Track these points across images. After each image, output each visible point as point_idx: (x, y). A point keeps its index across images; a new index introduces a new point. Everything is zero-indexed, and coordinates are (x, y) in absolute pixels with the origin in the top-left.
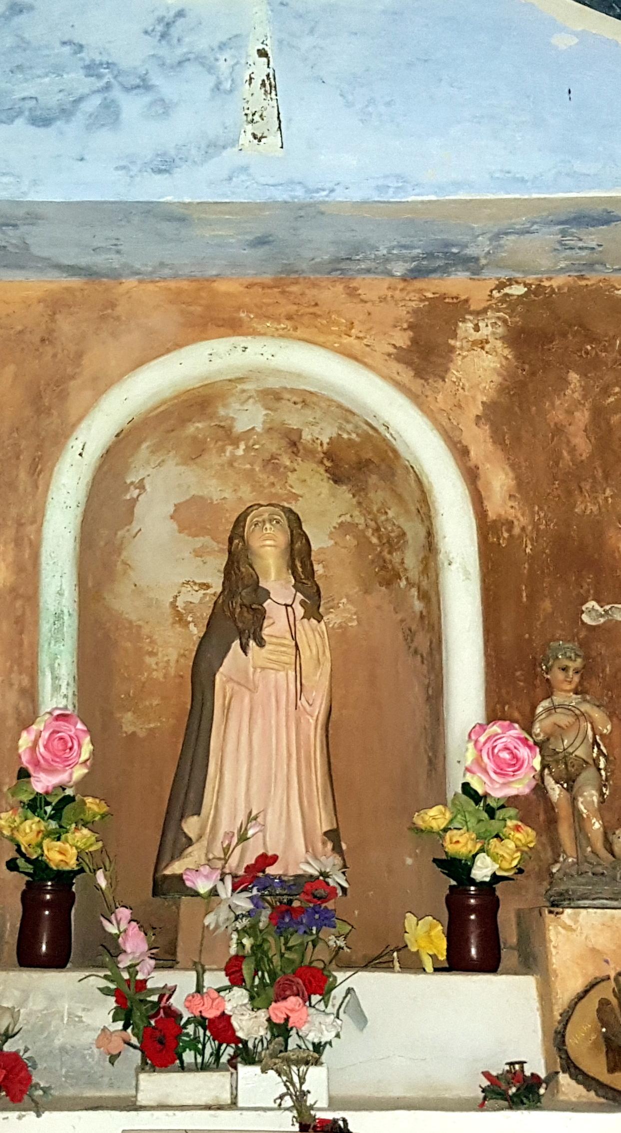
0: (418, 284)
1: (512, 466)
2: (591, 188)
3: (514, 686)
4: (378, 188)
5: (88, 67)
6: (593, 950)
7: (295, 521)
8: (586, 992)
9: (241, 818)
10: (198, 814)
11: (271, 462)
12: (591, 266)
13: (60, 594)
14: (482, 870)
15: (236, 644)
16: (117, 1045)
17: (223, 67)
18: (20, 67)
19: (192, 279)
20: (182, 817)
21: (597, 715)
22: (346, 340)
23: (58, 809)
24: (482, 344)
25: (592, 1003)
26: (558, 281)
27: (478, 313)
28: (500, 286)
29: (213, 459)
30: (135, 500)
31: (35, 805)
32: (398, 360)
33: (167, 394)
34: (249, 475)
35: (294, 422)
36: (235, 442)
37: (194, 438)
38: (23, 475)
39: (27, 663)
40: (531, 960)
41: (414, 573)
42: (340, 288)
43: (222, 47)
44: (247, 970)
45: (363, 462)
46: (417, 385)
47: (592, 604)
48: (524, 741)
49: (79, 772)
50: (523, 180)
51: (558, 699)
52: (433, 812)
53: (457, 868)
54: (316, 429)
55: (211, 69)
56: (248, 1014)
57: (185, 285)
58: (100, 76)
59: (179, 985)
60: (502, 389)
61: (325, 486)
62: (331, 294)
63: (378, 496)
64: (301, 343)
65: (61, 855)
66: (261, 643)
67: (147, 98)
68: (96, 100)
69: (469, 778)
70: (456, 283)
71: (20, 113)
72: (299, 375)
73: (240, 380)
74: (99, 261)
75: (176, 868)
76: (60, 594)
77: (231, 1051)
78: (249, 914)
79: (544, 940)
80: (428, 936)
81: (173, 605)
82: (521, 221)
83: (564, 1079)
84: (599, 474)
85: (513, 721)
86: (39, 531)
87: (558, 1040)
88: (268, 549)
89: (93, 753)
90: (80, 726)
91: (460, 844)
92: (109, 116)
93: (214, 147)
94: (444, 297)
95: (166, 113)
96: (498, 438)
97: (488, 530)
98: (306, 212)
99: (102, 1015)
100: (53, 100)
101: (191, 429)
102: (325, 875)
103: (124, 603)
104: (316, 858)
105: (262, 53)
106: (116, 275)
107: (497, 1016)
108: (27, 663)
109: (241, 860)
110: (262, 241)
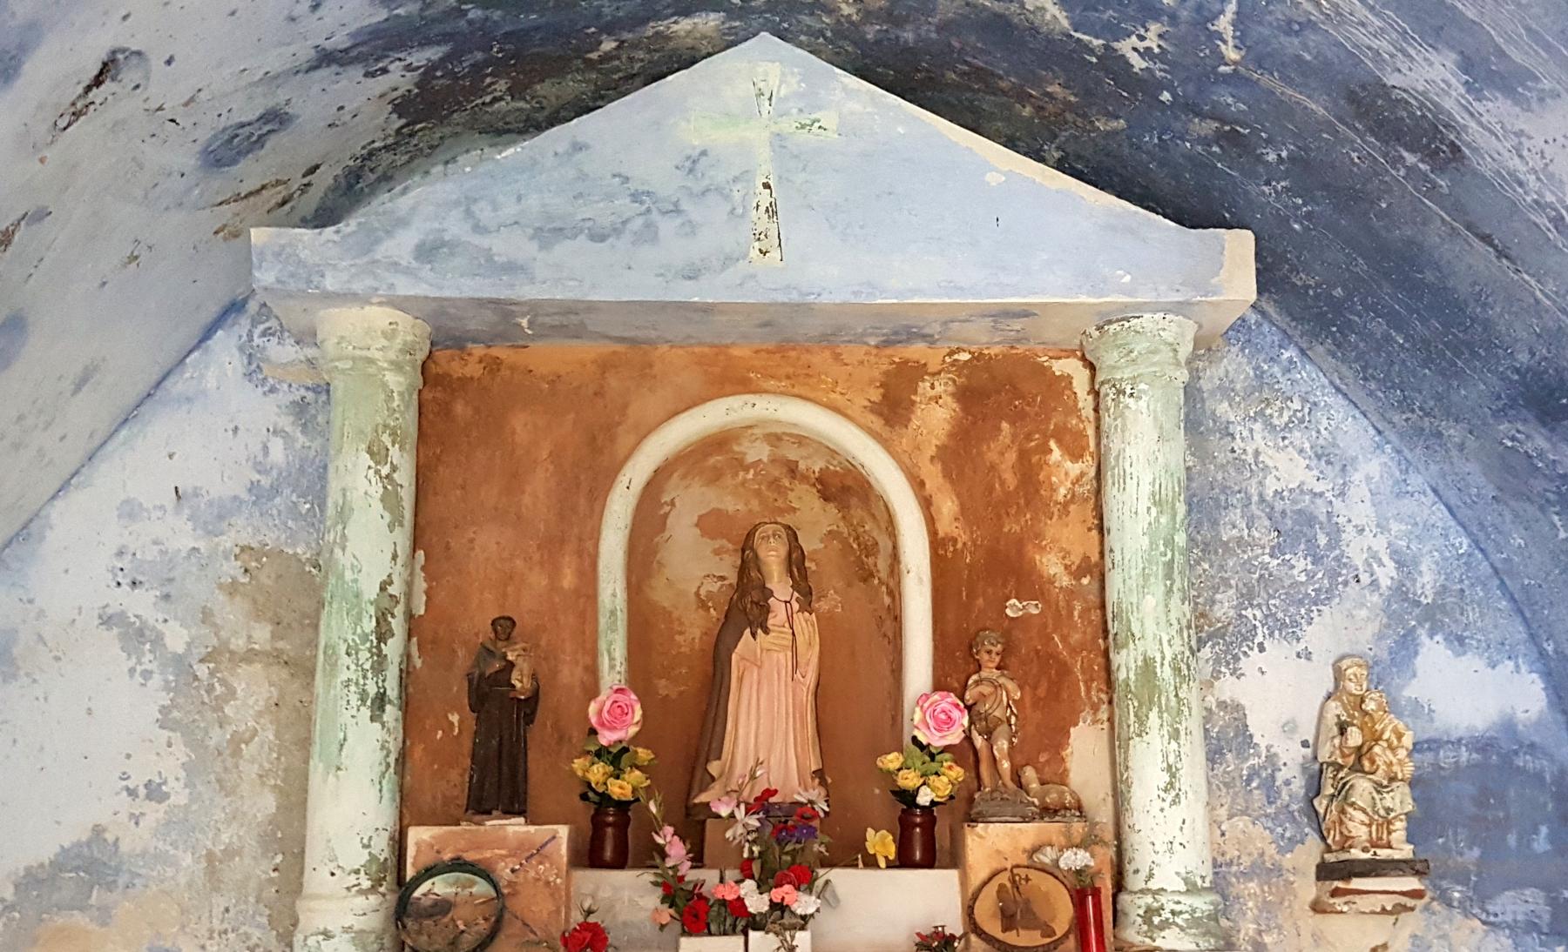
0: (889, 351)
1: (958, 496)
2: (1013, 296)
3: (955, 665)
4: (854, 293)
5: (632, 195)
6: (998, 852)
7: (792, 535)
8: (990, 879)
9: (751, 763)
10: (719, 758)
11: (774, 484)
12: (1018, 340)
13: (614, 595)
14: (924, 798)
15: (748, 631)
16: (666, 919)
17: (737, 196)
18: (581, 195)
19: (712, 346)
20: (707, 761)
21: (1011, 685)
22: (833, 396)
23: (616, 758)
24: (937, 399)
25: (993, 888)
26: (994, 351)
27: (933, 374)
28: (951, 354)
29: (728, 480)
30: (666, 515)
31: (601, 753)
32: (872, 411)
33: (695, 438)
34: (758, 493)
35: (792, 456)
36: (747, 470)
37: (715, 467)
38: (582, 501)
39: (588, 646)
40: (955, 860)
41: (884, 574)
42: (827, 354)
43: (735, 180)
44: (756, 868)
45: (845, 488)
46: (885, 432)
47: (1013, 601)
48: (957, 706)
49: (633, 730)
50: (962, 289)
51: (984, 674)
52: (891, 756)
53: (907, 797)
54: (809, 462)
55: (727, 198)
56: (756, 896)
57: (706, 350)
58: (642, 203)
59: (708, 878)
60: (951, 435)
61: (817, 503)
62: (820, 359)
63: (857, 513)
64: (798, 401)
65: (620, 789)
66: (766, 631)
67: (679, 221)
68: (639, 222)
69: (916, 733)
70: (916, 351)
71: (582, 231)
72: (795, 425)
73: (750, 427)
74: (640, 334)
75: (703, 798)
76: (614, 595)
77: (743, 923)
78: (757, 830)
79: (964, 845)
80: (881, 842)
81: (697, 594)
82: (963, 315)
83: (973, 938)
84: (1022, 501)
85: (949, 690)
86: (596, 546)
87: (969, 911)
88: (773, 556)
89: (644, 715)
90: (633, 697)
91: (909, 780)
92: (649, 234)
93: (729, 260)
94: (906, 362)
95: (694, 233)
96: (947, 474)
97: (937, 544)
98: (802, 309)
99: (652, 900)
100: (606, 221)
101: (711, 461)
102: (811, 802)
103: (660, 595)
104: (806, 790)
105: (767, 186)
106: (651, 343)
107: (931, 896)
108: (588, 646)
109: (752, 793)
110: (766, 324)
